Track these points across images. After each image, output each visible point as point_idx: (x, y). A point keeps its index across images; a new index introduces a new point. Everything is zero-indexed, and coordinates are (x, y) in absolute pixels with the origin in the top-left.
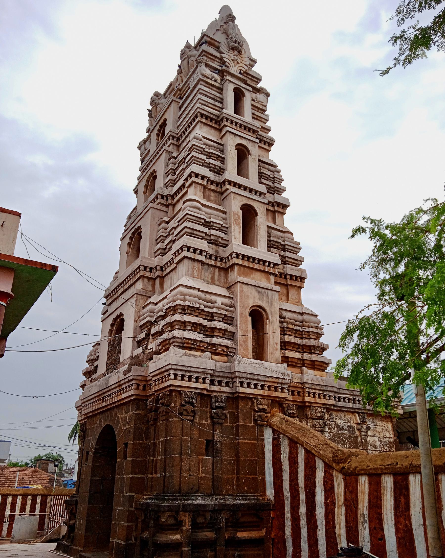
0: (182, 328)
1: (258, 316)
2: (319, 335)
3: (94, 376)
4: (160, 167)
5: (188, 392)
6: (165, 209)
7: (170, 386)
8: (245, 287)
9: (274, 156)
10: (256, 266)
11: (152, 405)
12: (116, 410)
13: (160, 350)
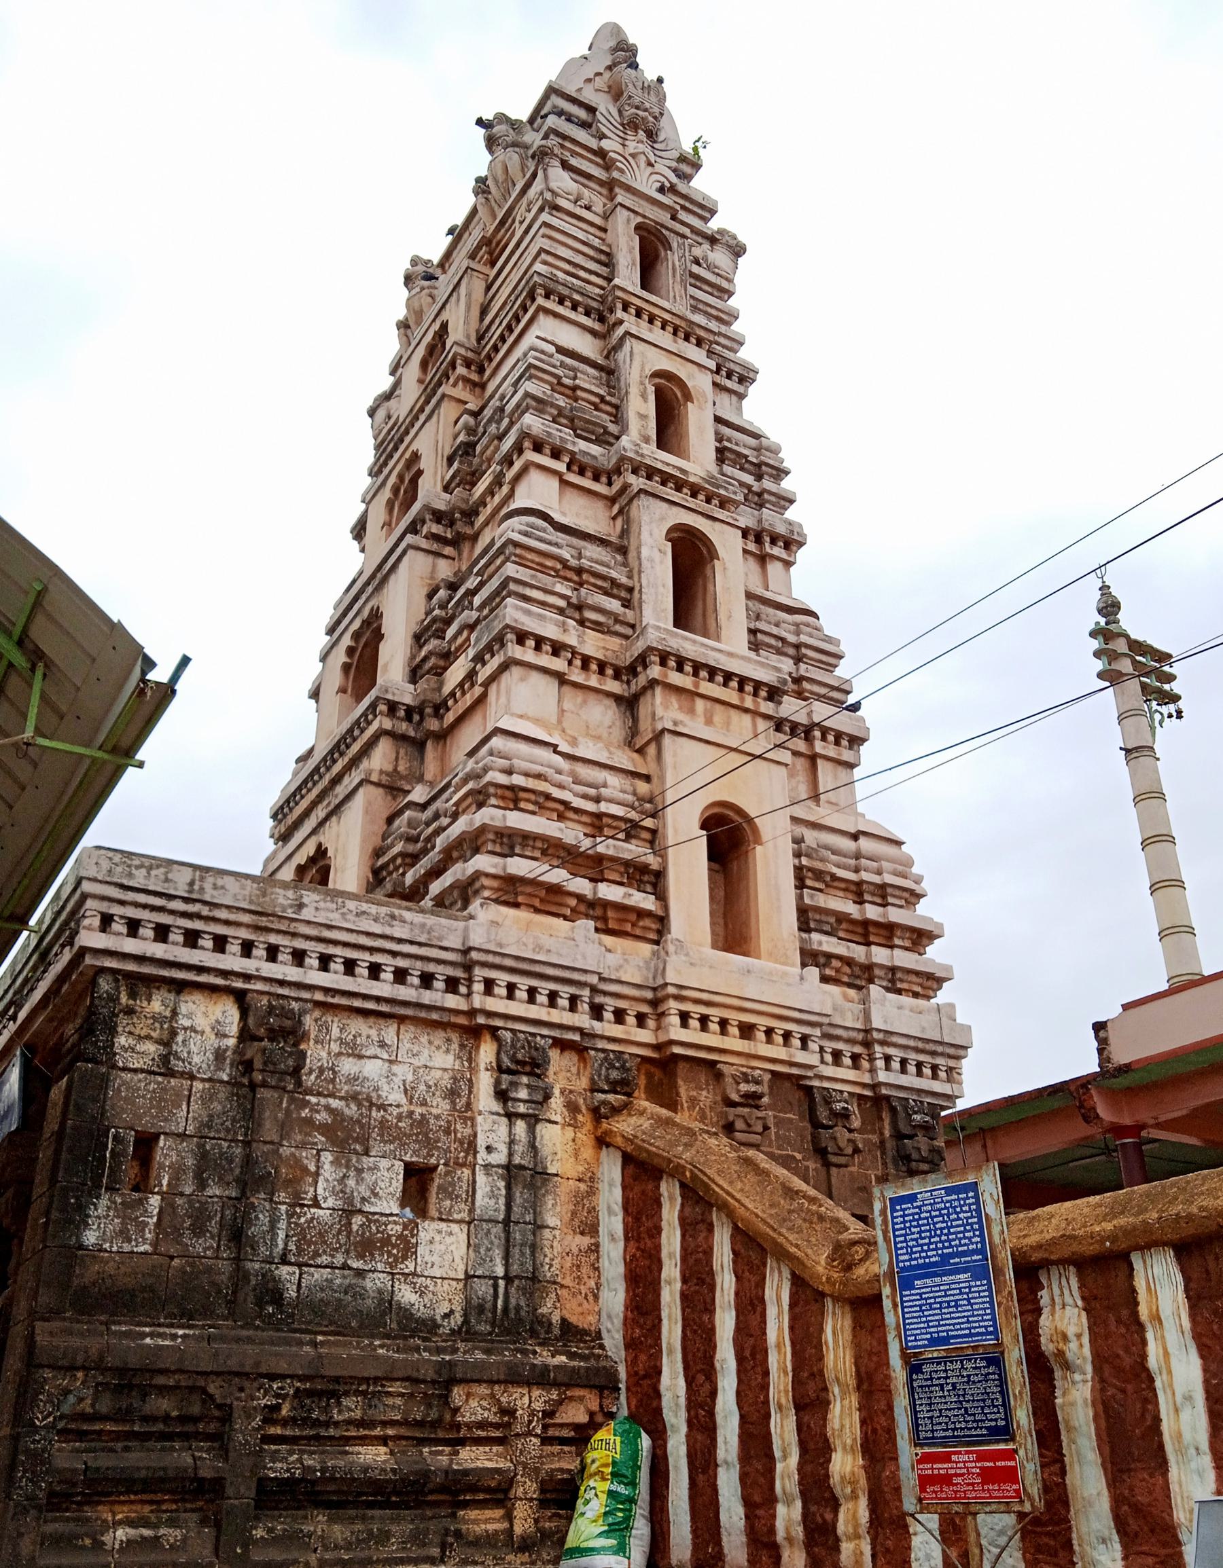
0: (506, 851)
1: (728, 837)
2: (912, 897)
9: (756, 410)
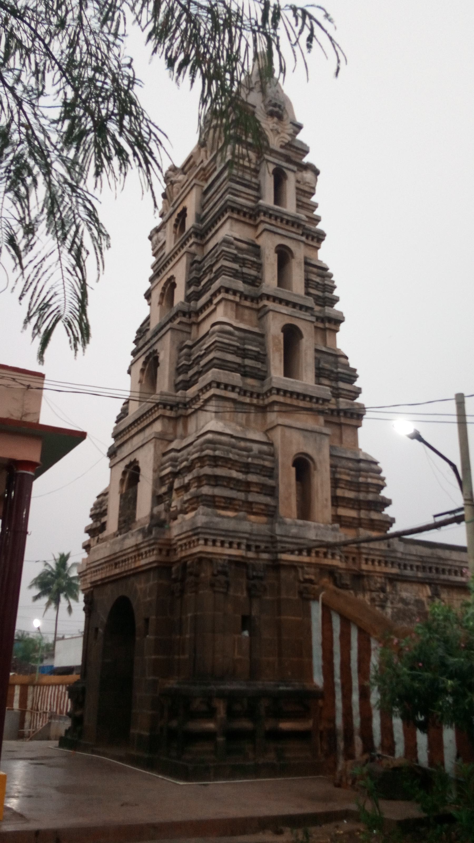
1: (303, 465)
3: (101, 536)
4: (180, 272)
5: (221, 559)
6: (187, 329)
7: (200, 552)
8: (288, 432)
10: (301, 404)
11: (177, 575)
12: (132, 579)
13: (186, 508)
